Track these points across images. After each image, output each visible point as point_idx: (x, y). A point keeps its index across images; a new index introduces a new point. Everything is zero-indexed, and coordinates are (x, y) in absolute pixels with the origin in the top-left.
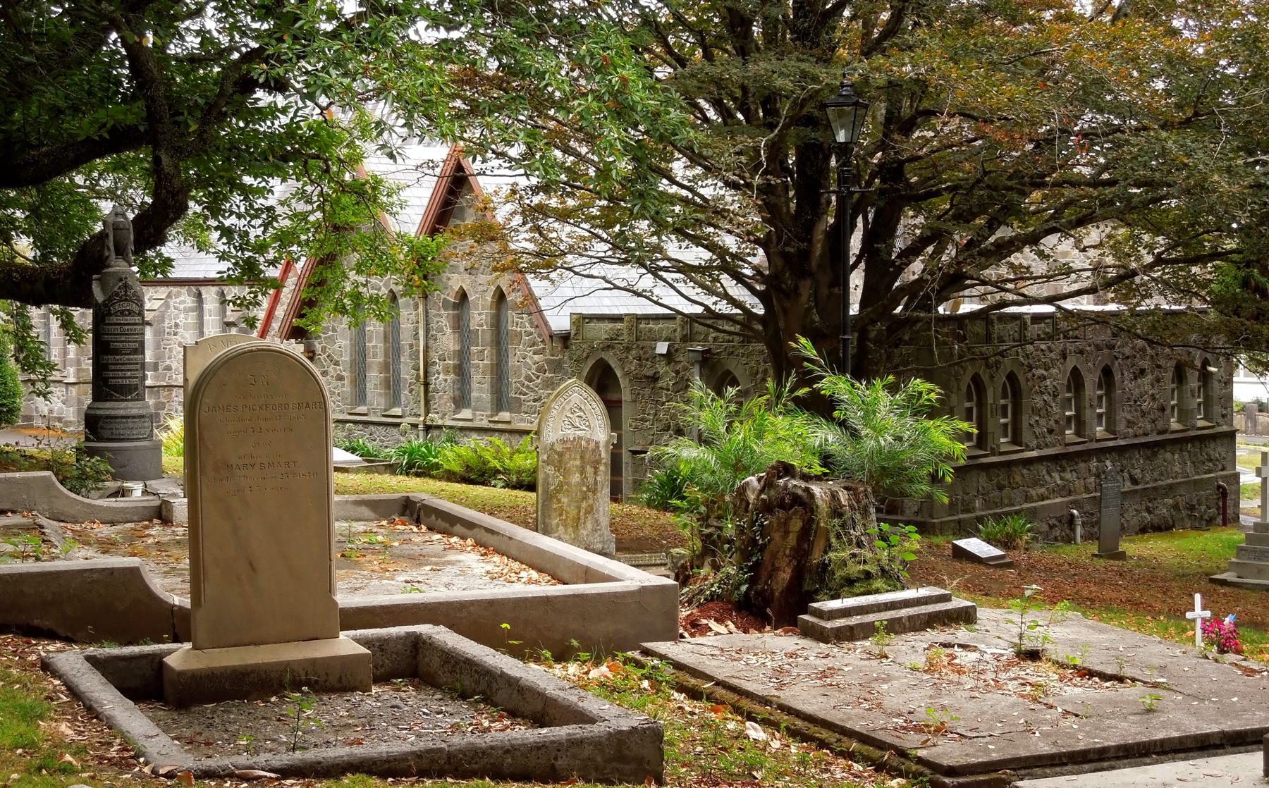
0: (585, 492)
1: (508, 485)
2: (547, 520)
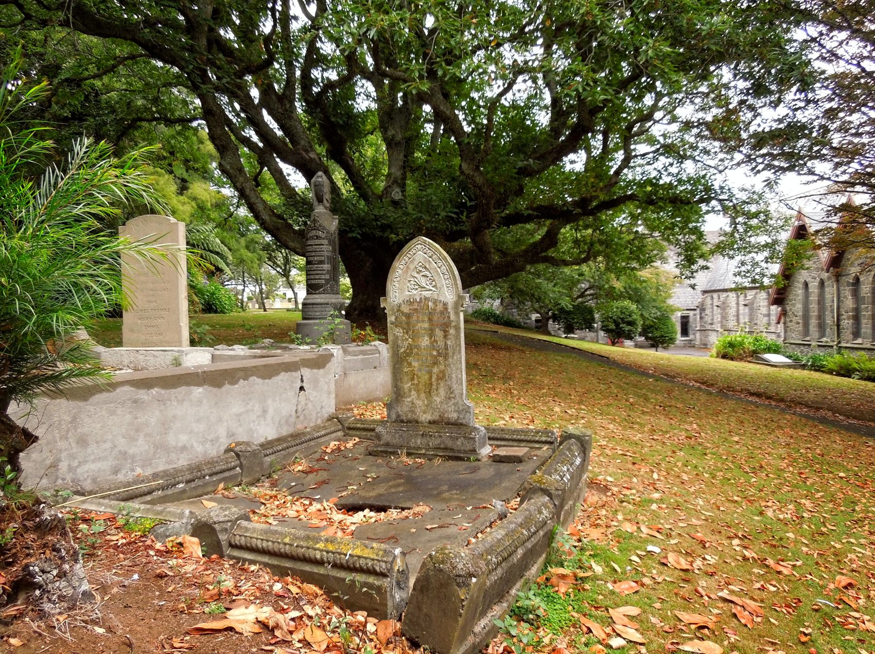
0: (436, 357)
1: (861, 379)
2: (399, 383)
